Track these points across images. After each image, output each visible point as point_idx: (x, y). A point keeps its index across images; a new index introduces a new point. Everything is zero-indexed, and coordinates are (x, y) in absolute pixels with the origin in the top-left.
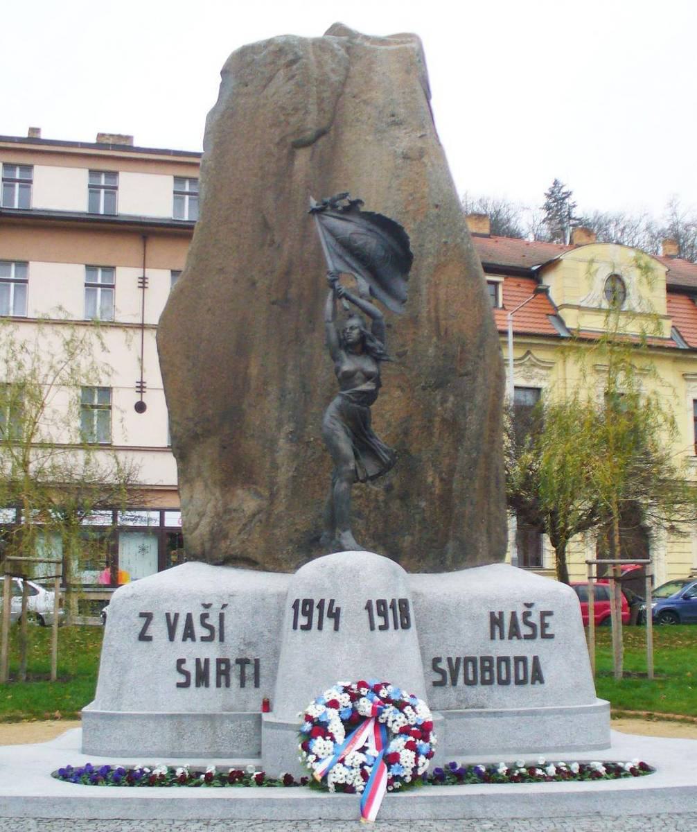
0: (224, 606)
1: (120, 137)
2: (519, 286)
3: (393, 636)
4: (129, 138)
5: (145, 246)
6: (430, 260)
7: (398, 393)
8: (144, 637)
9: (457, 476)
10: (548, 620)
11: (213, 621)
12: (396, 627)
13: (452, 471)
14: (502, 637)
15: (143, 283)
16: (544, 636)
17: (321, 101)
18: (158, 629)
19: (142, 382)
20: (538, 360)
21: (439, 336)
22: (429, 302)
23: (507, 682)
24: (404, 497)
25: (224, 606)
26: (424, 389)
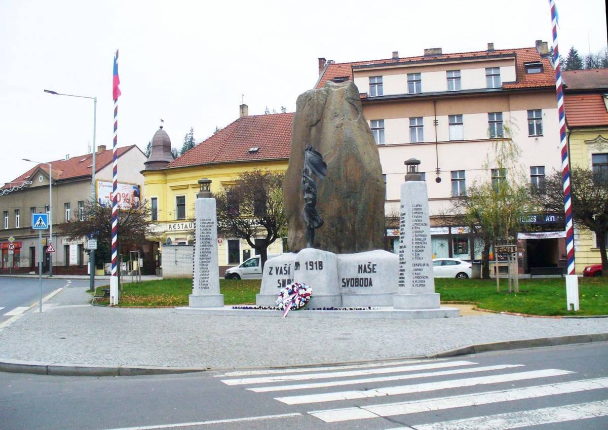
0: (290, 265)
1: (435, 49)
2: (583, 99)
3: (315, 272)
4: (440, 49)
5: (435, 106)
6: (343, 159)
7: (337, 200)
8: (270, 274)
9: (356, 224)
10: (375, 267)
11: (287, 269)
12: (317, 269)
13: (355, 222)
14: (362, 272)
15: (436, 123)
16: (373, 272)
17: (318, 111)
18: (274, 271)
19: (438, 169)
20: (604, 139)
21: (347, 182)
22: (344, 172)
23: (362, 286)
24: (341, 231)
25: (290, 265)
26: (344, 198)
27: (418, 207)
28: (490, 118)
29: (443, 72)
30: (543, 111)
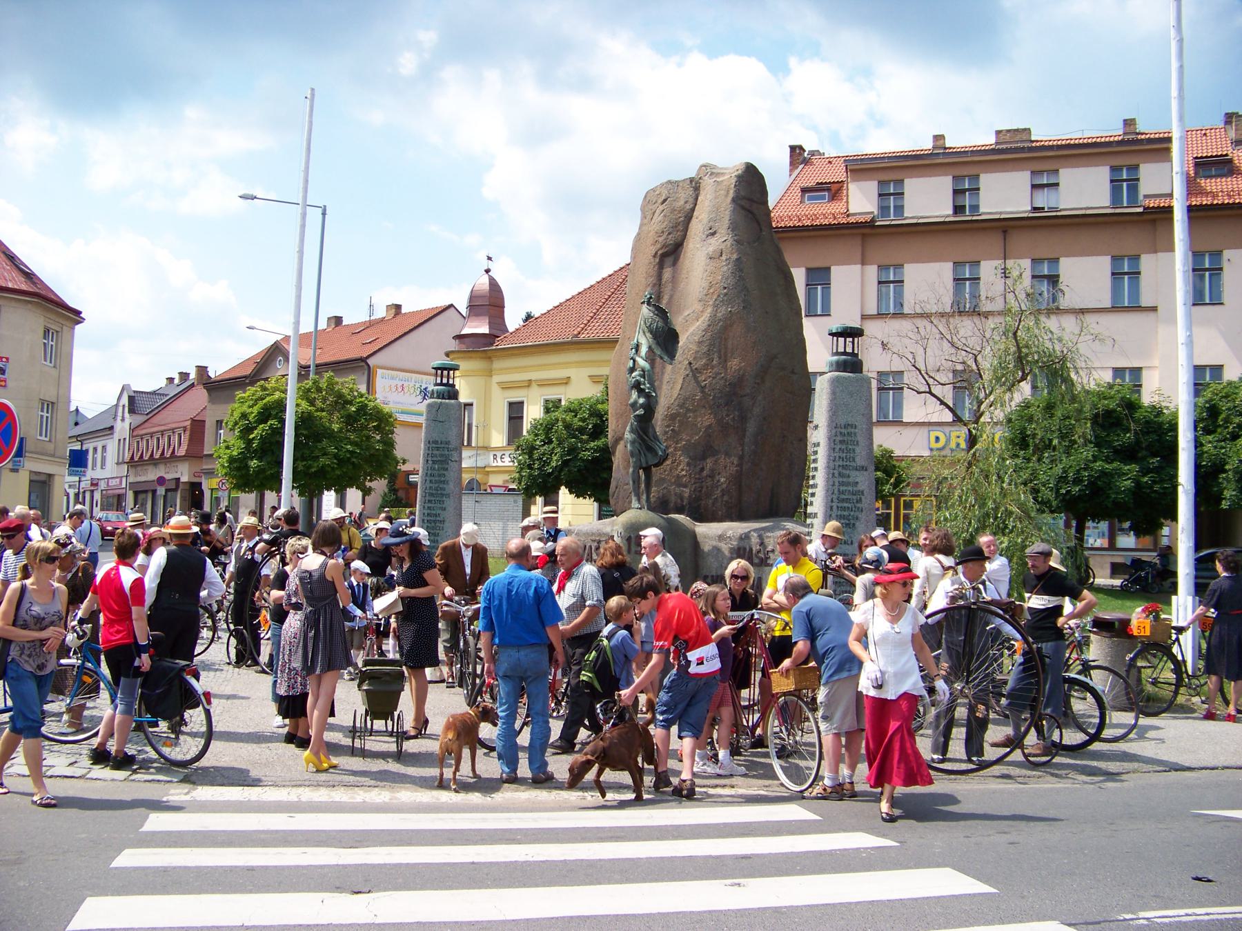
27: (850, 430)
28: (1113, 265)
29: (1101, 168)
30: (1227, 254)
